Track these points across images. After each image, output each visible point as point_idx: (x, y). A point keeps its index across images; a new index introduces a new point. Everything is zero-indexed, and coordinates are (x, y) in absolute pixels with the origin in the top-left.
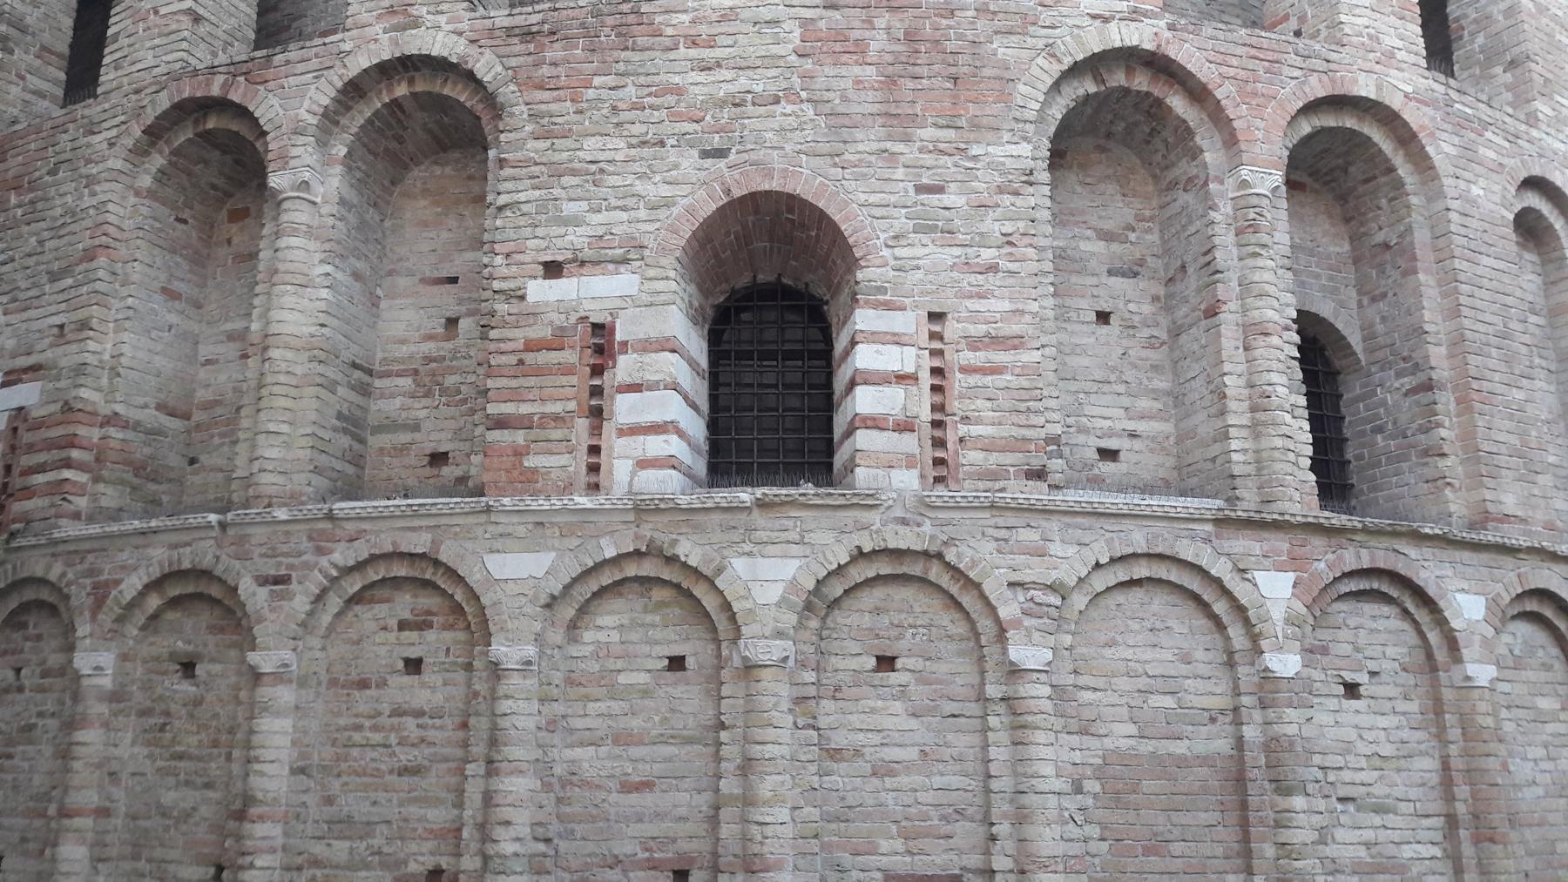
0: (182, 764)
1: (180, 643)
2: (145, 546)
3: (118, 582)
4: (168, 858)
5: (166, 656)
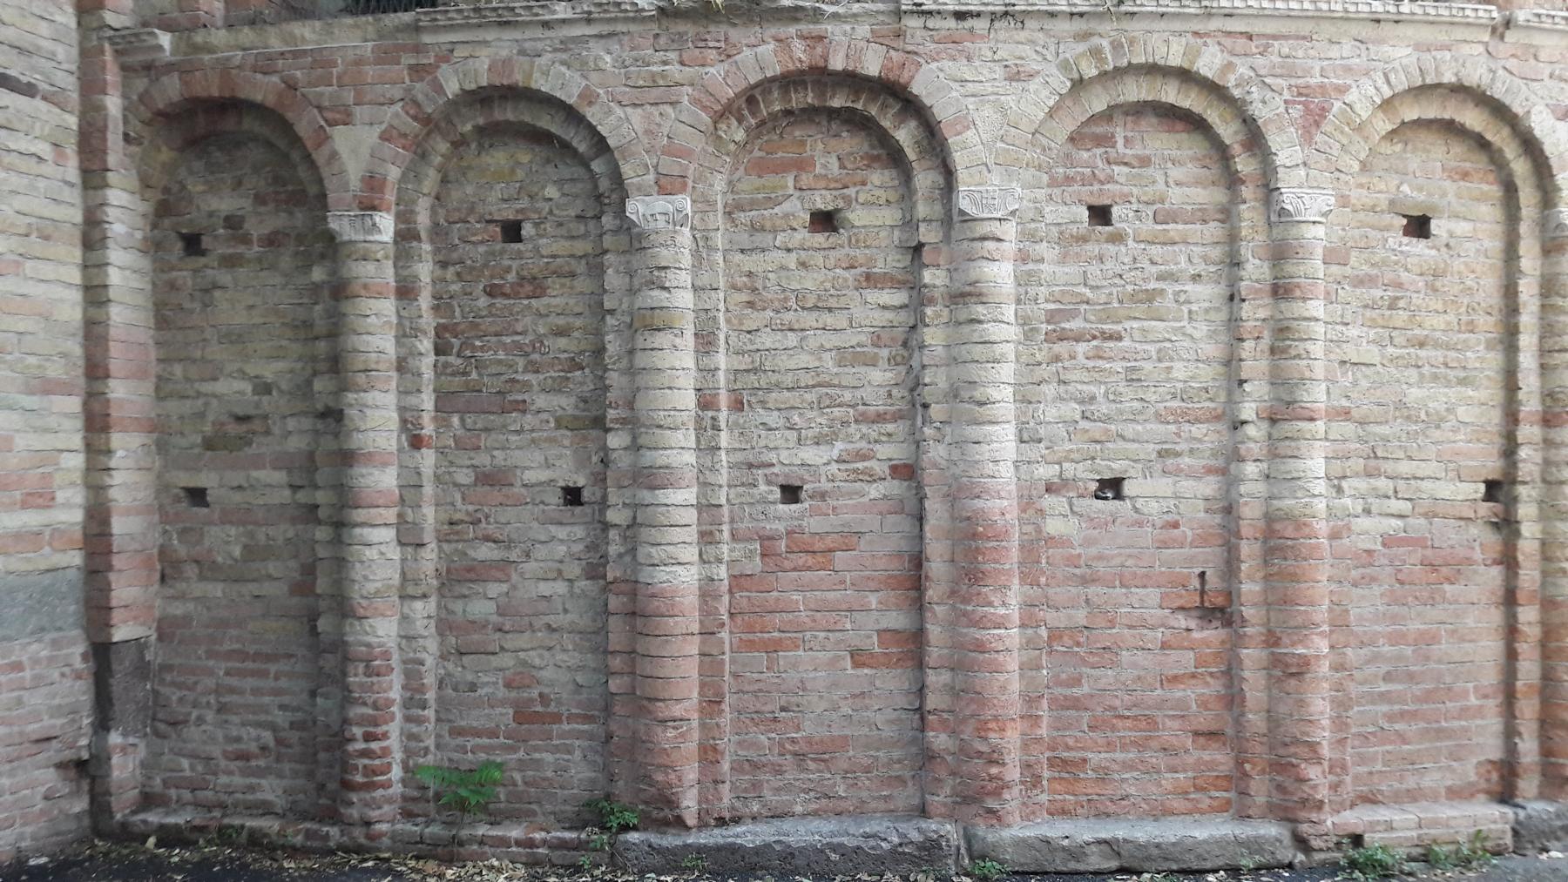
0: (1423, 353)
1: (1405, 188)
2: (1381, 41)
3: (1342, 90)
4: (1420, 474)
5: (1384, 205)
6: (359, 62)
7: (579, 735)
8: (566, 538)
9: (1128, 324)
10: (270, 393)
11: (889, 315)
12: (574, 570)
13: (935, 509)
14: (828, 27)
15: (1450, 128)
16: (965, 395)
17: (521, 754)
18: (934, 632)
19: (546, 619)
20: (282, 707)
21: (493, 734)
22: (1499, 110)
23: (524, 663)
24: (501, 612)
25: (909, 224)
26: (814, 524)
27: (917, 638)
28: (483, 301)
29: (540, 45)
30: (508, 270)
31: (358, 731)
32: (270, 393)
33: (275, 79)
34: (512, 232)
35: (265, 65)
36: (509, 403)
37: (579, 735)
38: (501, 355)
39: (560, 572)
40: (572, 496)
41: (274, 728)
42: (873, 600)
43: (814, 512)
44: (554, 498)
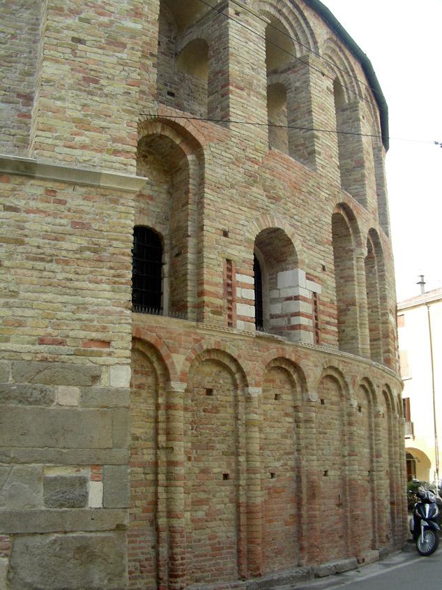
6: (180, 334)
7: (228, 553)
8: (226, 490)
9: (328, 430)
10: (138, 440)
11: (290, 425)
12: (227, 500)
13: (304, 480)
14: (285, 347)
15: (279, 368)
16: (310, 448)
17: (214, 561)
18: (303, 513)
19: (220, 516)
20: (142, 553)
21: (206, 555)
22: (341, 374)
23: (214, 532)
24: (207, 515)
25: (295, 400)
26: (278, 485)
27: (299, 516)
28: (203, 414)
29: (227, 339)
30: (209, 404)
31: (179, 557)
32: (138, 440)
33: (154, 334)
34: (209, 392)
35: (151, 329)
36: (209, 447)
37: (228, 553)
38: (207, 431)
39: (223, 501)
40: (226, 476)
41: (140, 561)
42: (289, 506)
43: (277, 481)
44: (222, 477)
